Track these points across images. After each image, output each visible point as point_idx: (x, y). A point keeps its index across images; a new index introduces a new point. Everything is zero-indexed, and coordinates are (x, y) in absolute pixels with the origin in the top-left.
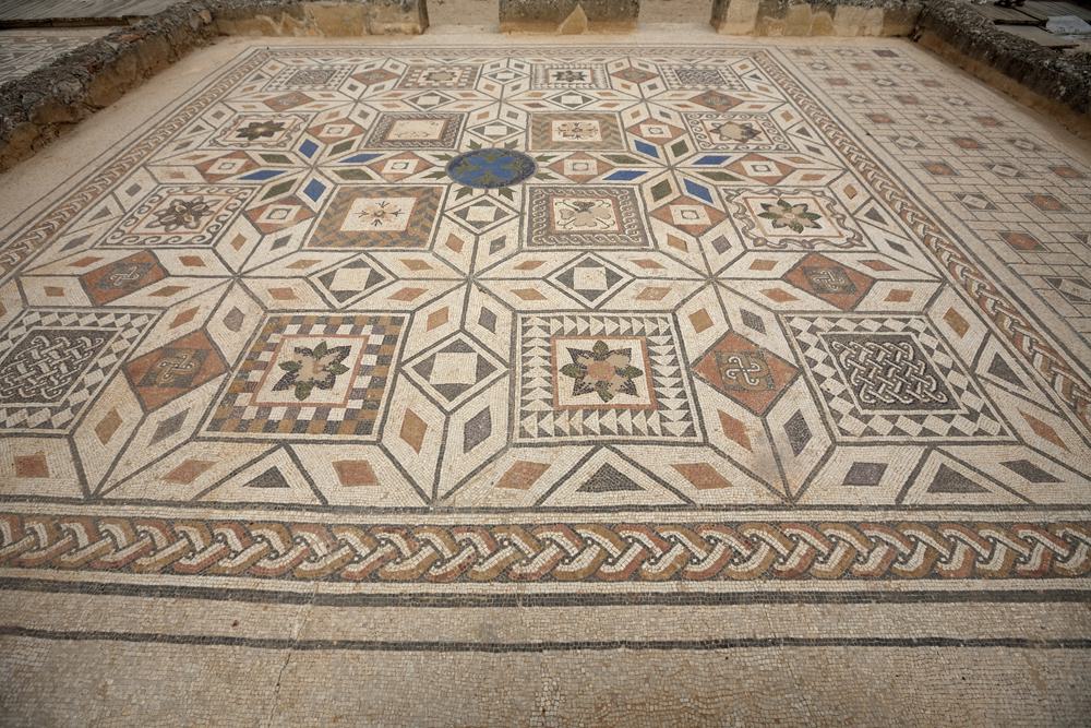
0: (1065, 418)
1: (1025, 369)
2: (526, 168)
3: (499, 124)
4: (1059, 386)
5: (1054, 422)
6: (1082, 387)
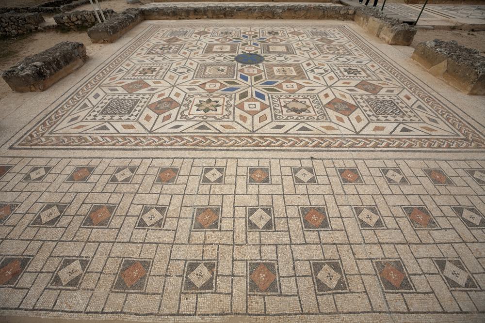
0: (79, 133)
1: (100, 133)
2: (238, 59)
3: (184, 68)
4: (88, 138)
5: (80, 130)
6: (84, 144)
